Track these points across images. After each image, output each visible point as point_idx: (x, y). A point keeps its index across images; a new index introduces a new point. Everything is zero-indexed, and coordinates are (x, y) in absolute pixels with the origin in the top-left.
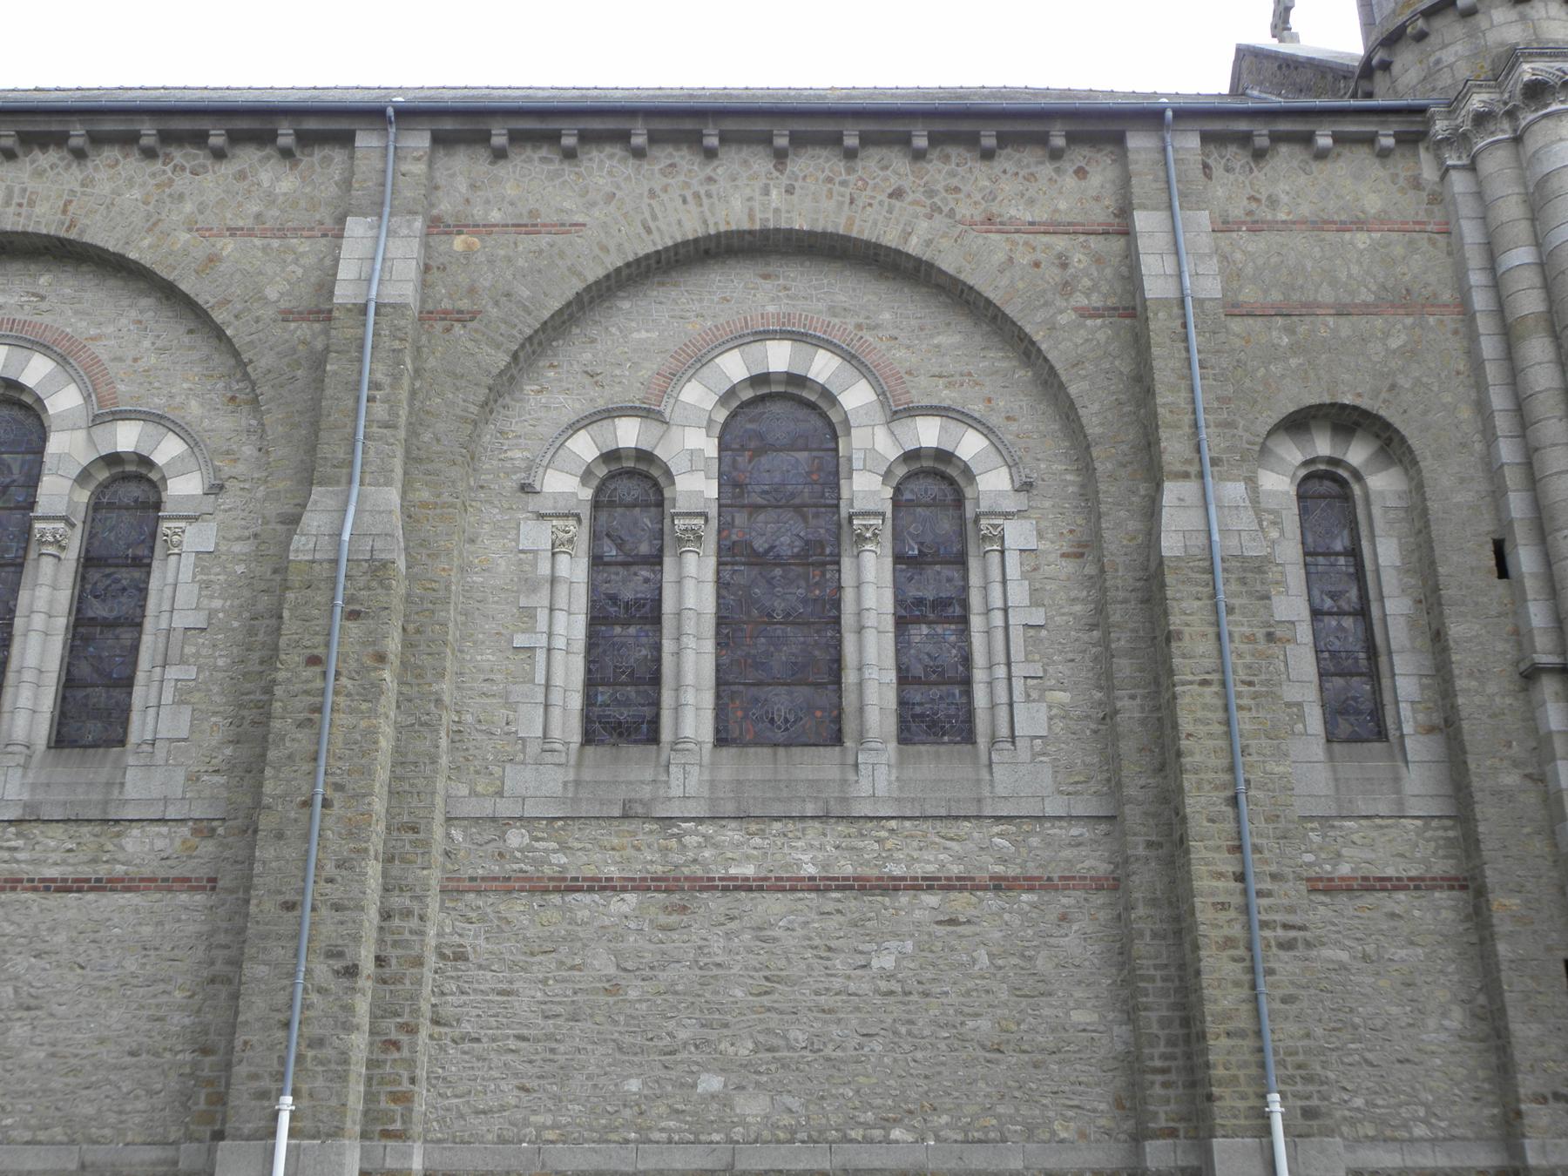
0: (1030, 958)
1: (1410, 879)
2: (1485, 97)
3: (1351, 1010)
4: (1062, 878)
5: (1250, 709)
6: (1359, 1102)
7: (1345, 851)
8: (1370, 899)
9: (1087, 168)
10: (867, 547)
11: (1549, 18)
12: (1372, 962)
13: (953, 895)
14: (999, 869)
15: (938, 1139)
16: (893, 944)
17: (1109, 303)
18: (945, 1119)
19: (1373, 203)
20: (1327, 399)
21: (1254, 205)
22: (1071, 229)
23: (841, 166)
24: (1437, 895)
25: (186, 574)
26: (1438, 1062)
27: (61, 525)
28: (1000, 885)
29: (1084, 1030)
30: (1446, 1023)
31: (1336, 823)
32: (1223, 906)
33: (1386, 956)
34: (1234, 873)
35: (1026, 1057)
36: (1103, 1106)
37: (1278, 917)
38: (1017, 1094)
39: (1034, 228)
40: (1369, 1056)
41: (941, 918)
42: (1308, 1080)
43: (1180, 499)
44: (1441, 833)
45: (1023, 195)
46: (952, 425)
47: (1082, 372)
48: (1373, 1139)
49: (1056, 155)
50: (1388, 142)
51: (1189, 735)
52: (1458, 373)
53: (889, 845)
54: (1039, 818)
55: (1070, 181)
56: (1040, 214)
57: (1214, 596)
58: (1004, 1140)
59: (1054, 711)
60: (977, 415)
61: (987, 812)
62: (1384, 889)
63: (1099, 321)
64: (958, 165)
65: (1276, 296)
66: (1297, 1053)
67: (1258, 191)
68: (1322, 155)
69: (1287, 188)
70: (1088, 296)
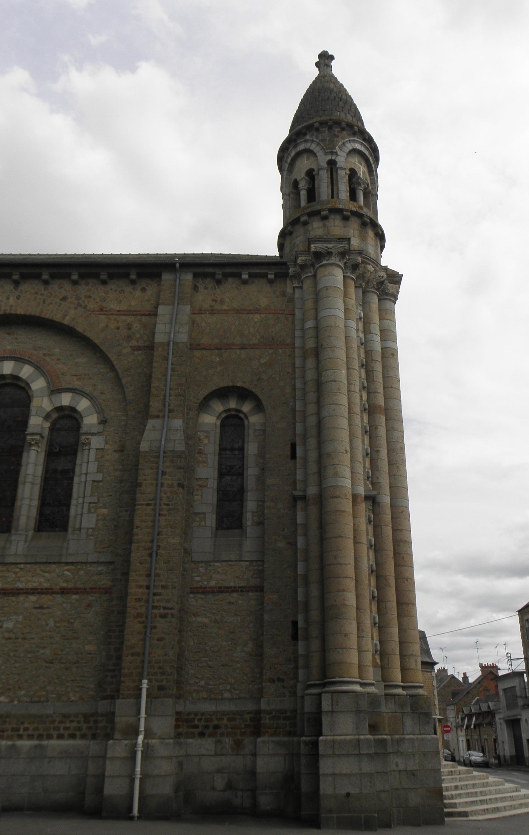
0: (72, 623)
1: (240, 587)
2: (303, 258)
3: (206, 644)
4: (90, 588)
5: (166, 516)
6: (202, 683)
7: (214, 576)
8: (221, 596)
9: (147, 288)
10: (32, 448)
11: (334, 226)
12: (218, 623)
13: (42, 596)
14: (65, 585)
15: (19, 701)
16: (14, 617)
17: (146, 344)
18: (23, 692)
19: (264, 302)
20: (230, 384)
21: (214, 303)
22: (135, 313)
23: (42, 287)
24: (250, 594)
25: (92, 457)
26: (239, 665)
27: (38, 437)
28: (64, 591)
29: (90, 654)
30: (245, 649)
31: (212, 564)
32: (139, 600)
33: (224, 620)
34: (146, 586)
35: (62, 665)
36: (92, 686)
37: (162, 604)
38: (57, 681)
39: (119, 313)
40: (210, 663)
41: (36, 606)
42: (163, 674)
43: (153, 427)
44: (256, 568)
45: (117, 299)
46: (77, 396)
47: (129, 374)
48: (205, 699)
49: (133, 282)
50: (15, 277)
51: (138, 527)
52: (288, 373)
53: (19, 575)
54: (85, 563)
55: (138, 293)
56: (123, 307)
57: (158, 468)
58: (47, 701)
59: (100, 517)
60: (88, 392)
61: (63, 560)
62: (227, 592)
63: (140, 352)
64: (92, 287)
65: (216, 341)
66: (160, 662)
67: (217, 298)
68: (245, 282)
69: (229, 296)
70: (137, 341)
